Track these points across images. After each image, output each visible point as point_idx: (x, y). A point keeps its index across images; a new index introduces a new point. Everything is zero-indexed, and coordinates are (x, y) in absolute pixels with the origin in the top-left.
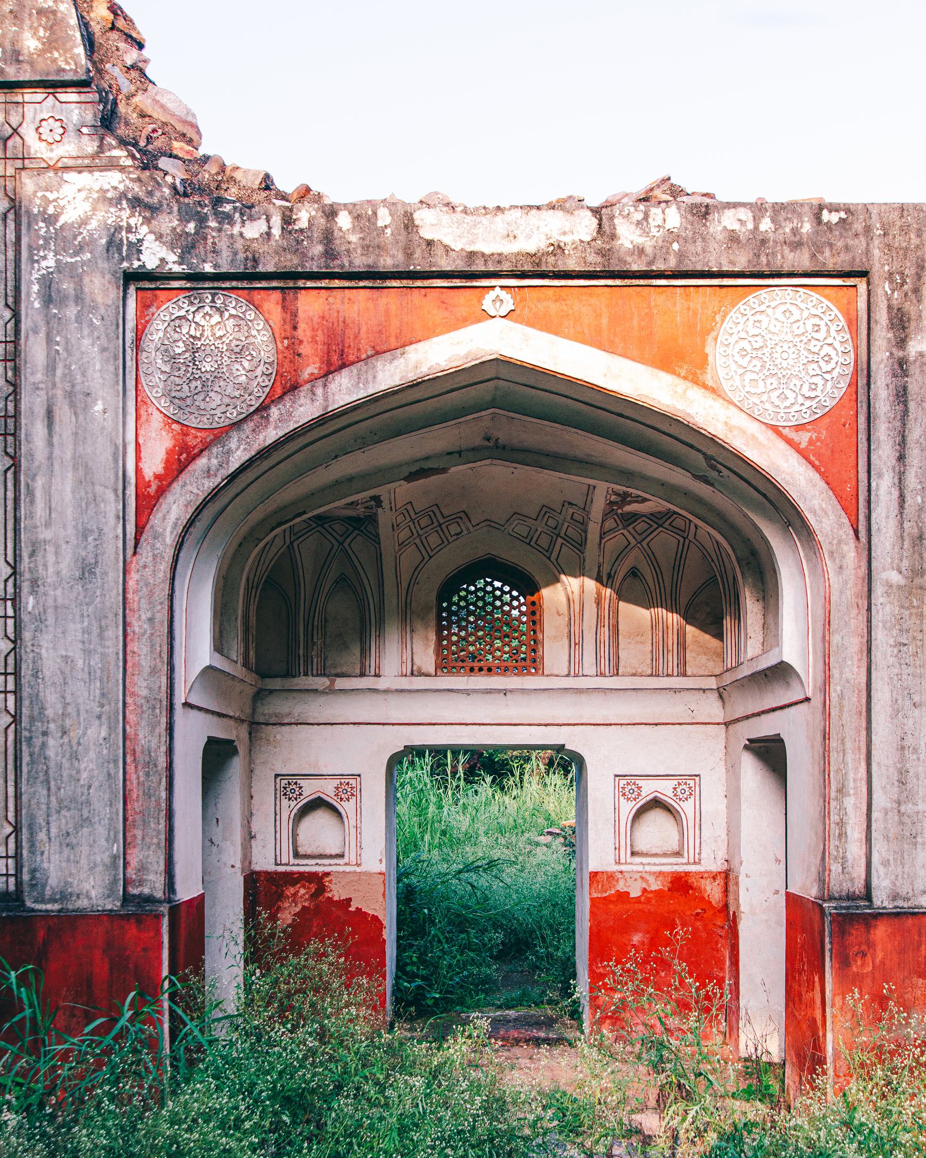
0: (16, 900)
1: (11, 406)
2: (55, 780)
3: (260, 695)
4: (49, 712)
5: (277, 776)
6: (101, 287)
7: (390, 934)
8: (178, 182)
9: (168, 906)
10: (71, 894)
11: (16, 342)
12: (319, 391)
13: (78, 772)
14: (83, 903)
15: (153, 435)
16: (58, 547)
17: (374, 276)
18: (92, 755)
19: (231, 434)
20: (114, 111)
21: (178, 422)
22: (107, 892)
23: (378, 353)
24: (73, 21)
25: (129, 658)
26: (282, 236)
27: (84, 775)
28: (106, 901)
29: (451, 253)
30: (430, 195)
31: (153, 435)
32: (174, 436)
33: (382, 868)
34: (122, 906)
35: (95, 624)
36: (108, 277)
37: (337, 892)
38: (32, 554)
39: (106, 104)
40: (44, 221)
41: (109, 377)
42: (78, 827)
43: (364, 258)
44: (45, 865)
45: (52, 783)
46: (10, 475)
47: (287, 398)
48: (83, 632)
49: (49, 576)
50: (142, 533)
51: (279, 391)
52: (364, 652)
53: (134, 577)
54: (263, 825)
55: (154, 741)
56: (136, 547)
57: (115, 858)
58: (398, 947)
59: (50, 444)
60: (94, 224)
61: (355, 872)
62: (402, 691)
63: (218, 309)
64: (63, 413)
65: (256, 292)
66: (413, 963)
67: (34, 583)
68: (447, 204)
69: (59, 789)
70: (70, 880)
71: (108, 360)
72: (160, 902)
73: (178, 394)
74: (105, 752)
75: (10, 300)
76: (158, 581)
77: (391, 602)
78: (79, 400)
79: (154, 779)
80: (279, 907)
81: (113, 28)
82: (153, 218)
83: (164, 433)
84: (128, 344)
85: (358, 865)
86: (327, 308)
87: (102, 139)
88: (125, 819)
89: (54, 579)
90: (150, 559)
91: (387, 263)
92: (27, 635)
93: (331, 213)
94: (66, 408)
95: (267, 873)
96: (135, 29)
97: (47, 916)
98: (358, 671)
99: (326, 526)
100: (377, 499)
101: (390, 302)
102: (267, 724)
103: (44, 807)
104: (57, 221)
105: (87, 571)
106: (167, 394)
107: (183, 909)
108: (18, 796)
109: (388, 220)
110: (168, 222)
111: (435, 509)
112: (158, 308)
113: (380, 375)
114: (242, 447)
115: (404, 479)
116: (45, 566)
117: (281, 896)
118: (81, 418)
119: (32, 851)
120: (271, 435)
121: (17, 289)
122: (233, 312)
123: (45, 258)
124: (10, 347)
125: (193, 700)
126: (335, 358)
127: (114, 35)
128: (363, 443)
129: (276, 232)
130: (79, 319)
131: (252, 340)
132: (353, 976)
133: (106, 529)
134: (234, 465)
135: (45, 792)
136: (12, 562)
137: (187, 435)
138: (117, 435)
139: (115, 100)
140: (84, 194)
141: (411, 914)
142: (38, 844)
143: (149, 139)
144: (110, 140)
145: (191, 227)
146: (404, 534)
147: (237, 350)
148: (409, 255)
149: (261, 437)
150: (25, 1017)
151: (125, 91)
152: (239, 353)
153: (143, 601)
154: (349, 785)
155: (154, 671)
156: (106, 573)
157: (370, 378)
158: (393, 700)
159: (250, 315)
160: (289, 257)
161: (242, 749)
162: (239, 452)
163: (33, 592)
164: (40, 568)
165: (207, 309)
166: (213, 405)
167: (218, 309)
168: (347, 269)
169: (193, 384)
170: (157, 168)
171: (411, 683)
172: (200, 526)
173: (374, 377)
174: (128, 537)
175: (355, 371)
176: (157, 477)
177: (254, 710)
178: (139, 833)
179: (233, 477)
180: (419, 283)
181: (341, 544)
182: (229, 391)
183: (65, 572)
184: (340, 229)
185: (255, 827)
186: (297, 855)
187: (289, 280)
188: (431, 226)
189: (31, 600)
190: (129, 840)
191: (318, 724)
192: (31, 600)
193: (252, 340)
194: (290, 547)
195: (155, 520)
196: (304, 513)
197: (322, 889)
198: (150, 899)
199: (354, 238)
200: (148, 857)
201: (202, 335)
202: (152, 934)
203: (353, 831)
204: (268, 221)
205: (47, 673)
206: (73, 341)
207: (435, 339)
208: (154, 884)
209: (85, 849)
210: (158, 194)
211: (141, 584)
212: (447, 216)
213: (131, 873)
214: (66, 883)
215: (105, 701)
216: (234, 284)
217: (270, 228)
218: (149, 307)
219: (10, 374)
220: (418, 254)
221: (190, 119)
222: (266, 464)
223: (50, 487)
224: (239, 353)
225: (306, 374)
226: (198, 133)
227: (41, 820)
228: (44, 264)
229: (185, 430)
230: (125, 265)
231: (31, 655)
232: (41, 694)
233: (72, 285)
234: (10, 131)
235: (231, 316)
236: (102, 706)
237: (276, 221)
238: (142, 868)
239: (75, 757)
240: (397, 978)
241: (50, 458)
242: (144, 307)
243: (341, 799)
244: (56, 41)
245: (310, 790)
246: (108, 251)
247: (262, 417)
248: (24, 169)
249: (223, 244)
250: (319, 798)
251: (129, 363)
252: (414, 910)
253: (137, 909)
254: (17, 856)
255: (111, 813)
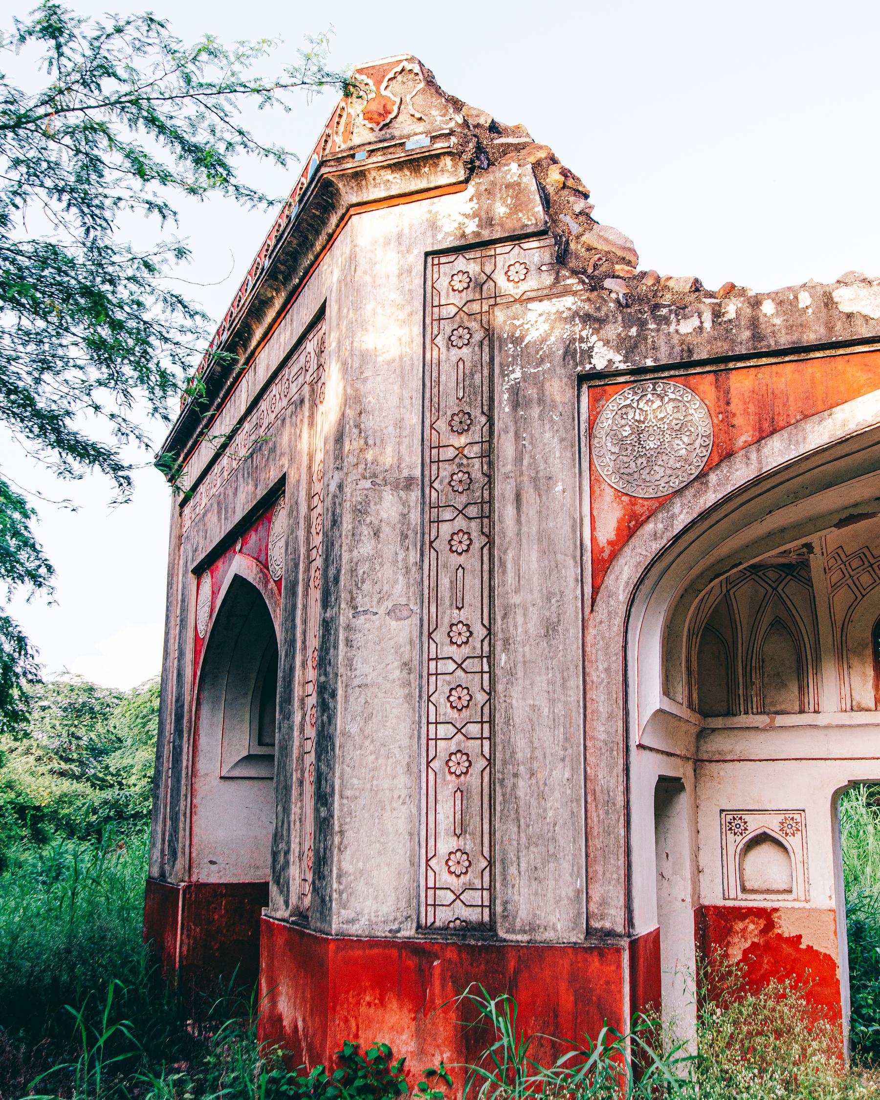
0: (490, 930)
1: (486, 494)
2: (525, 818)
3: (703, 734)
4: (519, 756)
5: (722, 811)
6: (559, 389)
7: (843, 974)
8: (621, 296)
9: (628, 940)
10: (539, 927)
11: (490, 442)
12: (753, 456)
13: (545, 810)
14: (549, 935)
15: (606, 507)
16: (526, 609)
17: (799, 351)
18: (557, 795)
19: (674, 500)
20: (566, 250)
21: (627, 495)
22: (572, 925)
23: (806, 417)
24: (534, 187)
25: (588, 705)
26: (713, 327)
27: (550, 814)
28: (571, 934)
29: (871, 322)
30: (846, 275)
31: (606, 507)
32: (624, 507)
33: (832, 904)
34: (586, 939)
35: (559, 676)
36: (565, 380)
37: (786, 928)
38: (505, 617)
39: (560, 245)
40: (512, 343)
41: (567, 462)
42: (545, 862)
43: (789, 337)
44: (516, 898)
45: (522, 821)
46: (486, 551)
47: (724, 465)
48: (548, 683)
49: (518, 634)
50: (597, 593)
51: (716, 459)
52: (802, 690)
53: (592, 631)
54: (710, 859)
55: (613, 781)
56: (592, 606)
57: (578, 892)
58: (852, 987)
59: (519, 521)
60: (553, 339)
61: (804, 908)
62: (843, 726)
63: (659, 395)
64: (529, 495)
65: (691, 378)
66: (869, 1006)
67: (506, 642)
68: (864, 280)
69: (528, 826)
70: (538, 912)
71: (566, 447)
72: (620, 936)
73: (626, 471)
74: (569, 791)
75: (486, 408)
76: (613, 634)
77: (826, 639)
78: (543, 484)
79: (614, 817)
80: (729, 942)
81: (564, 187)
82: (601, 328)
83: (615, 505)
84: (582, 433)
85: (807, 901)
86: (757, 383)
87: (558, 273)
88: (587, 856)
89: (523, 637)
90: (606, 615)
91: (810, 337)
92: (500, 687)
93: (756, 303)
94: (532, 491)
95: (715, 908)
96: (581, 184)
97: (517, 947)
98: (797, 708)
99: (760, 573)
100: (809, 547)
101: (815, 369)
102: (711, 761)
103: (515, 843)
104: (522, 341)
105: (550, 629)
106: (617, 471)
107: (642, 943)
108: (492, 833)
109: (809, 301)
110: (613, 330)
111: (865, 551)
112: (607, 400)
113: (810, 437)
114: (685, 511)
115: (835, 526)
116: (515, 626)
117: (729, 931)
118: (544, 498)
119: (505, 884)
120: (711, 498)
121: (491, 399)
122: (672, 396)
123: (513, 371)
124: (486, 446)
125: (646, 742)
126: (766, 425)
127: (566, 192)
128: (796, 497)
129: (708, 325)
130: (541, 417)
131: (690, 418)
132: (815, 1020)
133: (567, 592)
134: (678, 526)
135: (516, 829)
136: (487, 624)
137: (634, 504)
138: (575, 510)
139: (567, 241)
140: (543, 318)
141: (862, 952)
142: (509, 878)
143: (595, 267)
144: (564, 273)
145: (633, 331)
146: (836, 577)
147: (677, 427)
148: (830, 329)
149: (702, 501)
150: (502, 1046)
151: (574, 232)
152: (678, 431)
153: (600, 653)
154: (794, 820)
155: (610, 717)
156: (567, 630)
157: (801, 440)
158: (834, 734)
159: (688, 397)
160: (720, 344)
161: (688, 785)
162: (682, 515)
163: (505, 649)
164: (511, 628)
165: (649, 396)
166: (658, 477)
167: (659, 395)
168: (773, 347)
169: (639, 461)
170: (603, 288)
171: (851, 718)
172: (648, 583)
173: (805, 438)
174: (586, 597)
175: (786, 435)
176: (610, 543)
177: (698, 749)
178: (599, 869)
179: (677, 538)
180: (841, 351)
181: (775, 589)
182: (671, 463)
183: (532, 632)
184: (765, 315)
185: (703, 861)
186: (744, 890)
187: (721, 363)
188: (848, 300)
189: (504, 657)
190: (591, 875)
191: (760, 760)
192: (503, 657)
193: (690, 418)
194: (727, 596)
195: (610, 580)
196: (740, 563)
197: (770, 925)
198: (610, 933)
199: (778, 321)
200: (609, 891)
201: (645, 419)
202: (613, 968)
203: (800, 866)
204: (700, 317)
205: (517, 721)
206: (537, 435)
207: (860, 399)
208: (614, 920)
209: (551, 883)
210: (604, 309)
211: (598, 638)
212: (865, 291)
213: (593, 907)
214: (535, 915)
215: (568, 745)
216: (672, 373)
217: (701, 323)
218: (599, 400)
219: (485, 467)
220: (839, 326)
221: (628, 245)
222: (706, 524)
223: (519, 558)
224: (678, 431)
225: (740, 442)
226: (636, 255)
227: (512, 855)
228: (512, 376)
229: (633, 500)
230: (579, 368)
231: (504, 705)
232: (512, 740)
233: (535, 391)
234: (485, 278)
235: (670, 400)
236: (565, 749)
237: (707, 316)
238: (604, 903)
239: (542, 796)
240: (853, 1020)
241: (519, 534)
242: (595, 401)
243: (787, 834)
244: (520, 205)
245: (755, 825)
246: (564, 359)
247: (702, 483)
248: (496, 304)
249: (661, 342)
250: (765, 833)
251: (583, 449)
252: (865, 948)
253: (599, 942)
254: (491, 889)
255: (575, 849)
